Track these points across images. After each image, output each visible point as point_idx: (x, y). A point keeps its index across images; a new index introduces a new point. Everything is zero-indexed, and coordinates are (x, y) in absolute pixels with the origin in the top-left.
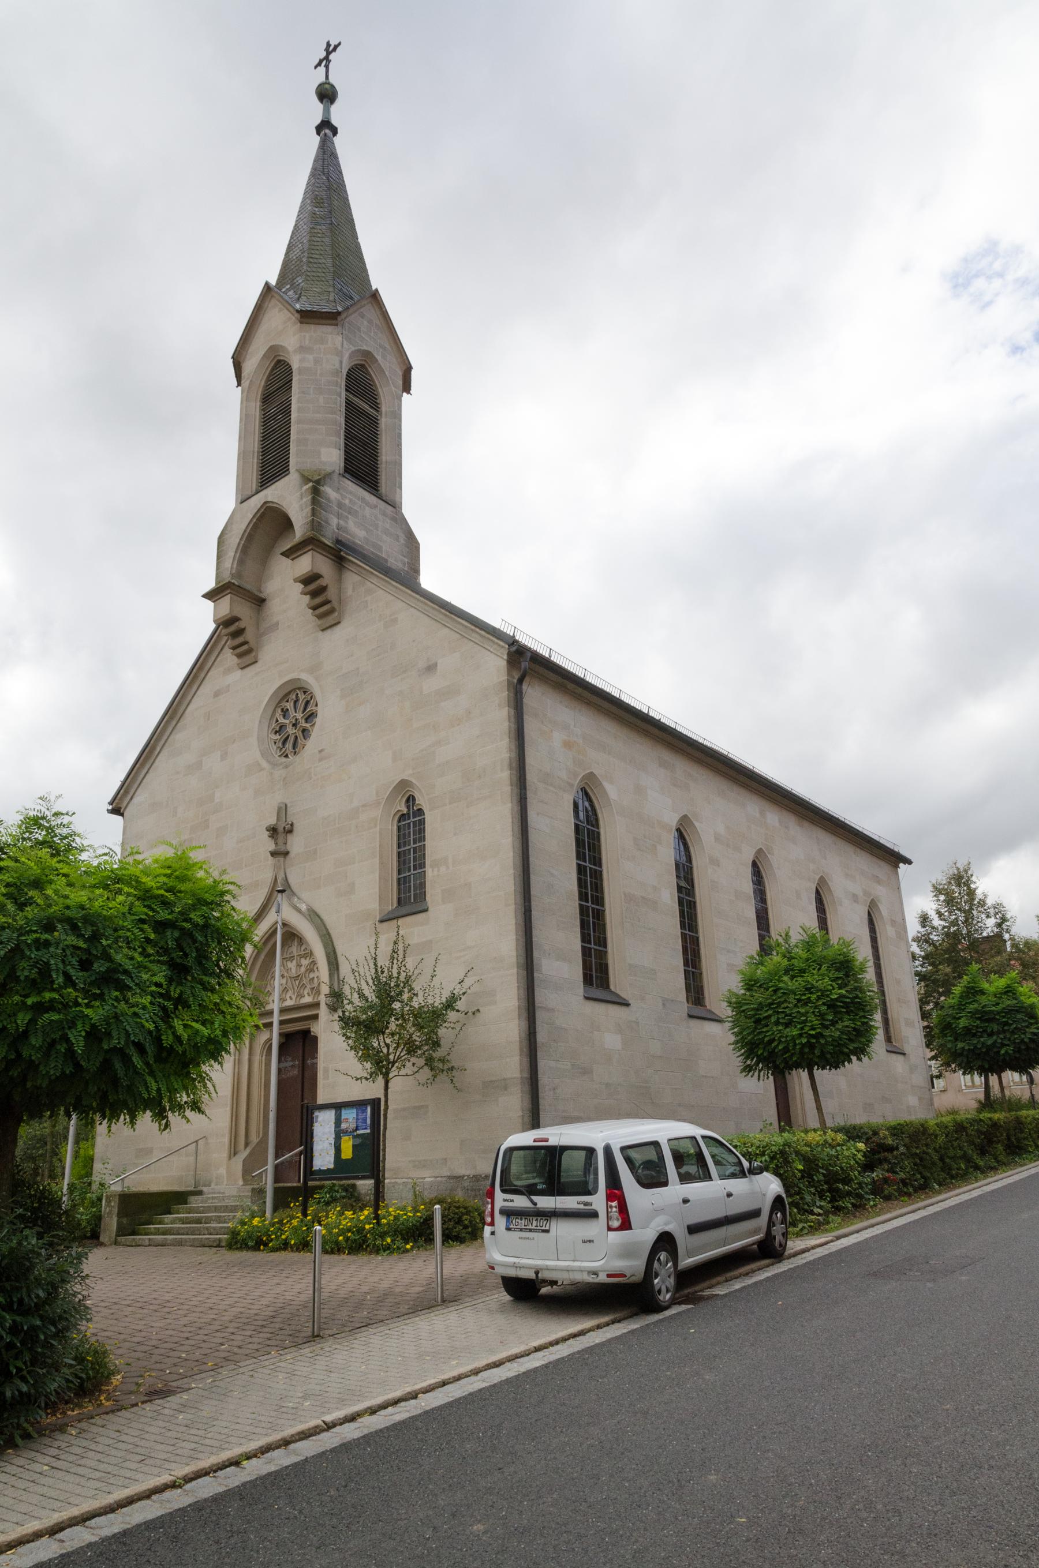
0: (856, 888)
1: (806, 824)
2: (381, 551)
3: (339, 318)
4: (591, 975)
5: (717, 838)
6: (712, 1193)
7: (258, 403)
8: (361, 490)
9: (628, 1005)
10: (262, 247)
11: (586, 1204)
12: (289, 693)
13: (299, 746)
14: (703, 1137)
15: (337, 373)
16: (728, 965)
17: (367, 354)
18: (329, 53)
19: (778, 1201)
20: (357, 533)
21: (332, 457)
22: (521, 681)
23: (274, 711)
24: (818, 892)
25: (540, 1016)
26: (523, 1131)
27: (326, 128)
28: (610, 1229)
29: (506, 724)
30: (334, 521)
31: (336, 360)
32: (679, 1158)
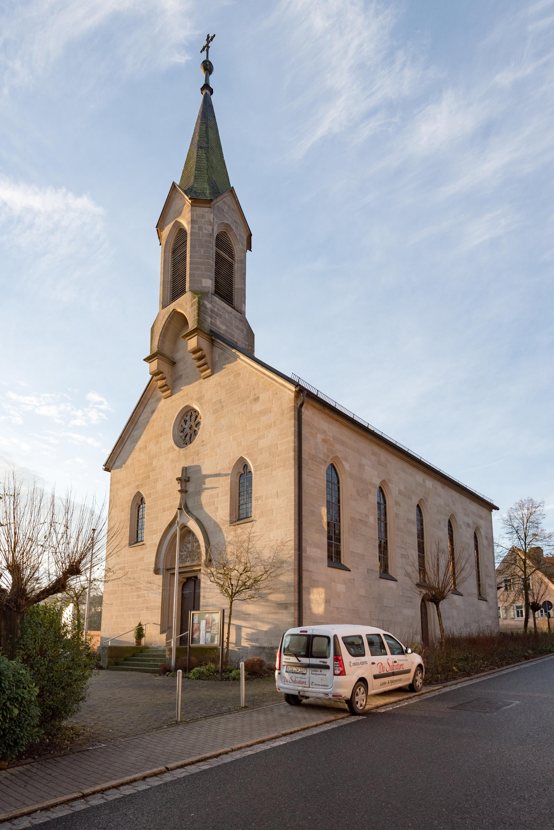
0: (469, 520)
1: (446, 487)
2: (234, 338)
3: (212, 204)
4: (332, 556)
5: (400, 492)
6: (387, 660)
7: (170, 254)
8: (223, 303)
9: (350, 571)
10: (172, 163)
11: (324, 662)
12: (188, 412)
13: (192, 438)
14: (384, 635)
15: (211, 235)
16: (401, 554)
17: (227, 225)
18: (208, 42)
19: (420, 666)
20: (221, 327)
21: (208, 284)
22: (302, 405)
23: (181, 421)
24: (449, 521)
25: (305, 574)
26: (294, 627)
27: (207, 88)
28: (335, 675)
29: (293, 429)
30: (209, 320)
31: (210, 228)
32: (371, 644)
